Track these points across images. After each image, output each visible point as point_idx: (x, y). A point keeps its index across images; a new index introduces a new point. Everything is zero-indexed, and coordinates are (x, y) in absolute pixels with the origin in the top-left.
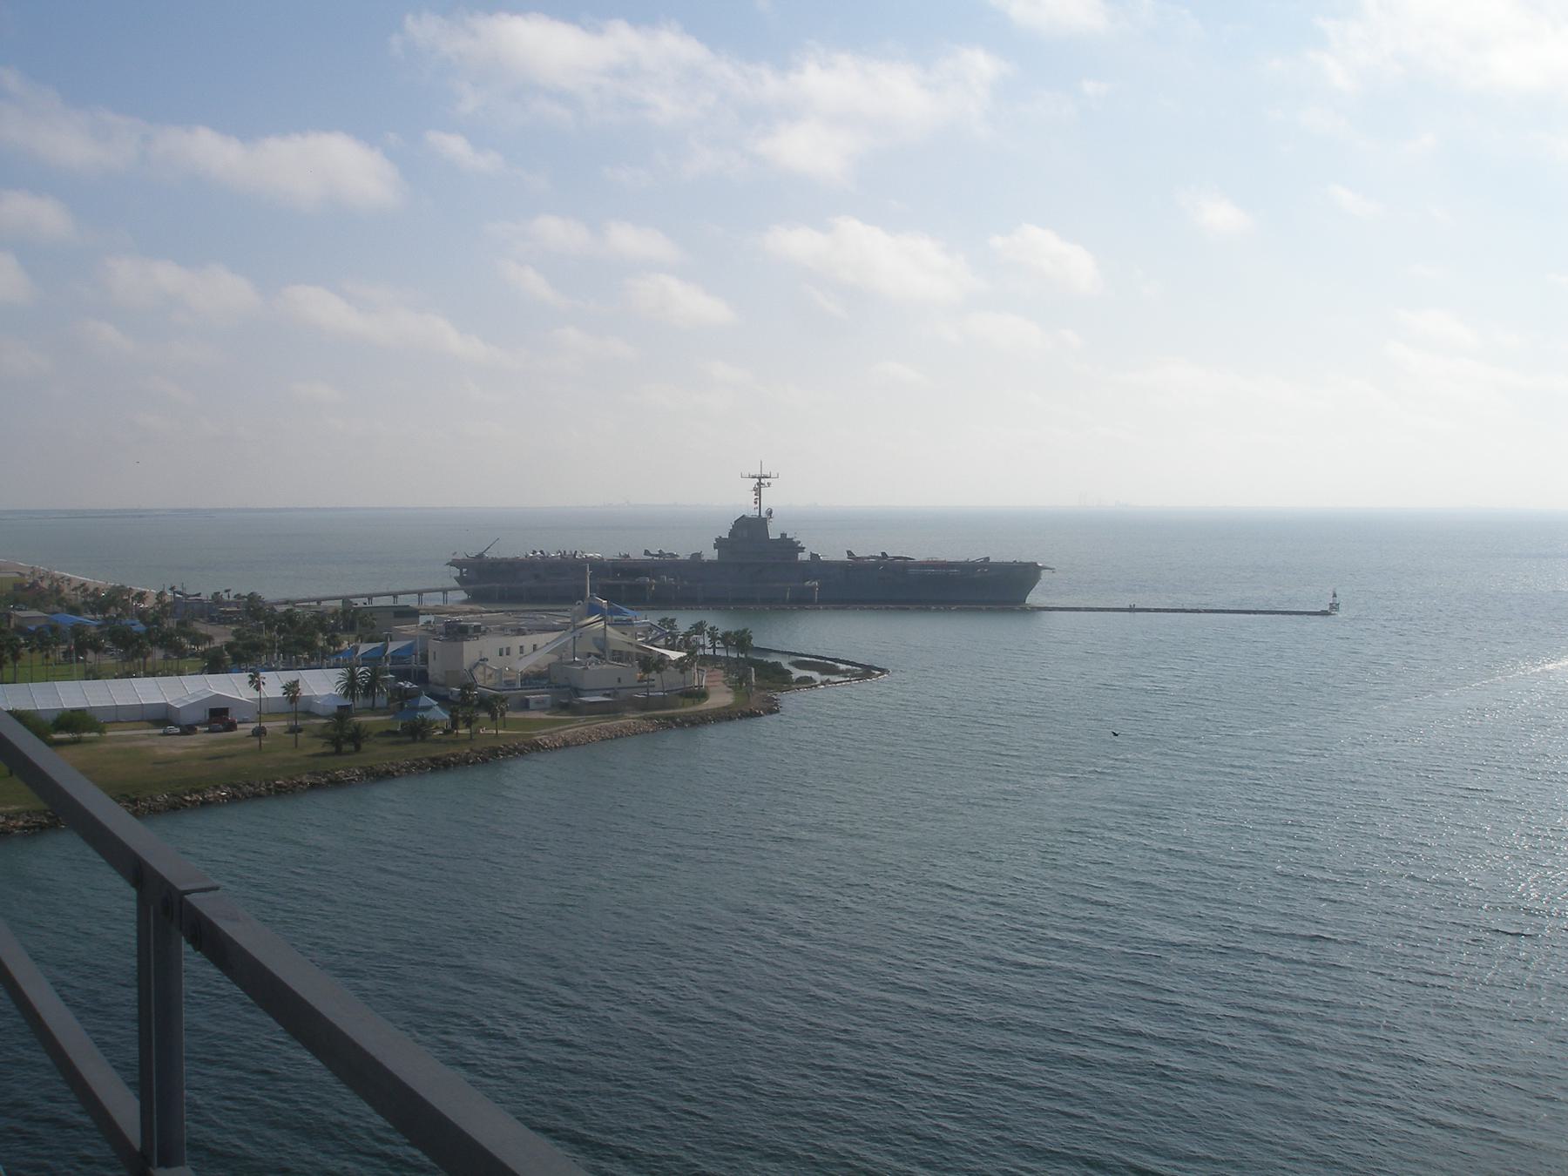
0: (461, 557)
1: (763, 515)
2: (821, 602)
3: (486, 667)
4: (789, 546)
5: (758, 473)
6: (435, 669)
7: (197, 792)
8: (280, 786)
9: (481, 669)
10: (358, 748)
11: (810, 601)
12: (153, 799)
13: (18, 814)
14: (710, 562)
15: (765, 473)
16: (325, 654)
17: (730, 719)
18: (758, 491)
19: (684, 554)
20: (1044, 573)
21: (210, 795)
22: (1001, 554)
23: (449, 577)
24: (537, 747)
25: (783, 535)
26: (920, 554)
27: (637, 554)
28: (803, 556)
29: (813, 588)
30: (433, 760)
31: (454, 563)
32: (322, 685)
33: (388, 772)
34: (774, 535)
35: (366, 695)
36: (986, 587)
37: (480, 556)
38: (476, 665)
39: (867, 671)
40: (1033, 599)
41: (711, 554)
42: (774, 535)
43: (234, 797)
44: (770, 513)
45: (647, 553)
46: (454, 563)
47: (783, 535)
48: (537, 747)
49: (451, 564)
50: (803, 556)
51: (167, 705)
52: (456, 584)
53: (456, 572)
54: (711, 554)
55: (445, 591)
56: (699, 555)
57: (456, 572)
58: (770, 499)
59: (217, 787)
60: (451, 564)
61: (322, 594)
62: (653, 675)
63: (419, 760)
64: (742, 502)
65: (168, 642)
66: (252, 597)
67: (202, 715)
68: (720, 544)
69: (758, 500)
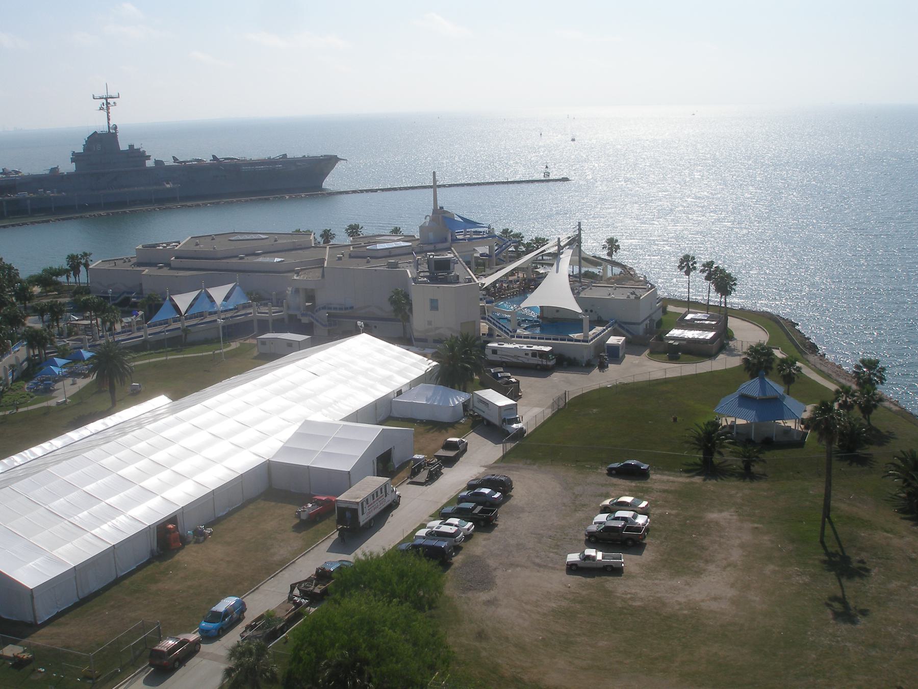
4: (136, 156)
5: (104, 95)
14: (69, 176)
22: (296, 151)
25: (131, 147)
28: (150, 163)
34: (123, 146)
36: (297, 177)
40: (330, 183)
41: (68, 167)
42: (123, 146)
47: (131, 147)
50: (150, 163)
68: (76, 158)
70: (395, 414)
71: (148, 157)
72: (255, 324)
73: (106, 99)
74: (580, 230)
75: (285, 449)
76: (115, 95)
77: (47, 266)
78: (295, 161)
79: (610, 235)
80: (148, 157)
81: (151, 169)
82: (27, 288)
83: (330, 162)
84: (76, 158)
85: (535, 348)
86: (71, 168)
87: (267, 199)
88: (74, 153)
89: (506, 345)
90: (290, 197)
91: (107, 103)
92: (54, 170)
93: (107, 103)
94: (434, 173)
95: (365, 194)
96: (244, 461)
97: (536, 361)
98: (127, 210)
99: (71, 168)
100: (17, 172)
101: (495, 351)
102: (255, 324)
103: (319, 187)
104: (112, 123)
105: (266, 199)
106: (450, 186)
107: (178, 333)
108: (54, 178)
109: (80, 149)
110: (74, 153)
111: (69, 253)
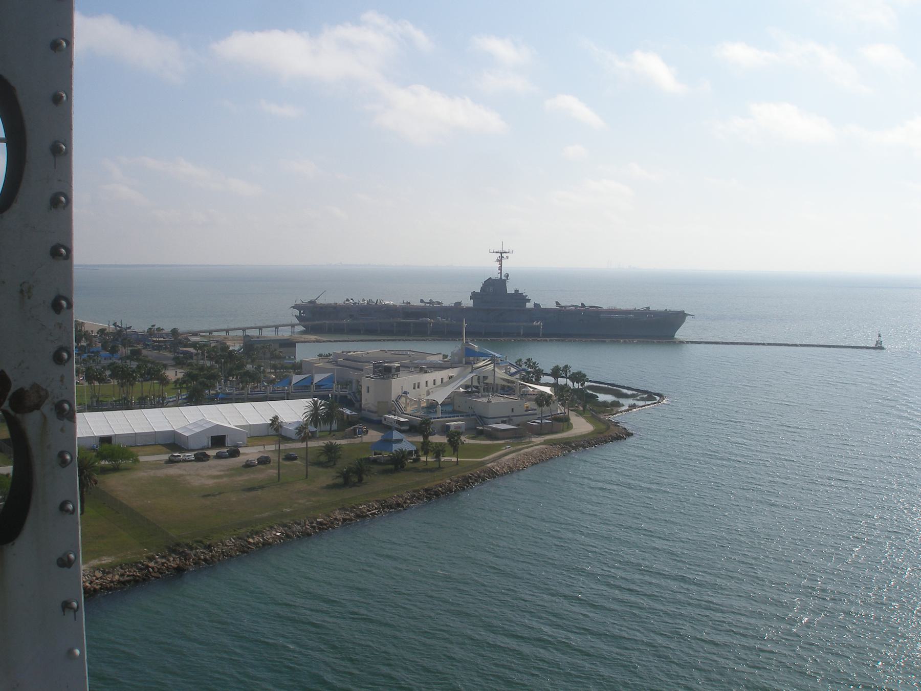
0: (299, 302)
1: (503, 278)
2: (544, 335)
3: (407, 398)
4: (520, 298)
5: (500, 250)
6: (368, 400)
7: (257, 533)
8: (321, 523)
9: (403, 400)
10: (360, 480)
11: (537, 335)
12: (224, 544)
13: (113, 567)
14: (468, 309)
16: (253, 377)
17: (606, 442)
18: (500, 261)
19: (448, 302)
20: (688, 317)
21: (268, 536)
22: (658, 305)
23: (291, 316)
24: (493, 474)
25: (517, 291)
27: (416, 302)
28: (529, 305)
29: (538, 327)
30: (426, 490)
32: (293, 412)
33: (398, 505)
34: (510, 290)
35: (325, 422)
36: (654, 327)
37: (311, 302)
38: (400, 397)
39: (651, 396)
40: (680, 335)
41: (468, 303)
42: (510, 290)
43: (288, 536)
45: (422, 301)
47: (517, 291)
48: (493, 474)
50: (529, 305)
51: (174, 433)
52: (297, 322)
53: (297, 312)
54: (468, 303)
55: (293, 326)
56: (460, 303)
59: (272, 527)
61: (212, 328)
62: (545, 408)
63: (417, 491)
64: (488, 267)
66: (174, 332)
67: (207, 442)
68: (474, 296)
69: (500, 269)
71: (529, 301)
78: (657, 313)
80: (529, 301)
81: (530, 310)
82: (159, 371)
84: (474, 296)
86: (469, 303)
87: (604, 342)
91: (501, 256)
93: (501, 256)
95: (761, 346)
96: (168, 428)
99: (469, 303)
100: (439, 303)
108: (457, 310)
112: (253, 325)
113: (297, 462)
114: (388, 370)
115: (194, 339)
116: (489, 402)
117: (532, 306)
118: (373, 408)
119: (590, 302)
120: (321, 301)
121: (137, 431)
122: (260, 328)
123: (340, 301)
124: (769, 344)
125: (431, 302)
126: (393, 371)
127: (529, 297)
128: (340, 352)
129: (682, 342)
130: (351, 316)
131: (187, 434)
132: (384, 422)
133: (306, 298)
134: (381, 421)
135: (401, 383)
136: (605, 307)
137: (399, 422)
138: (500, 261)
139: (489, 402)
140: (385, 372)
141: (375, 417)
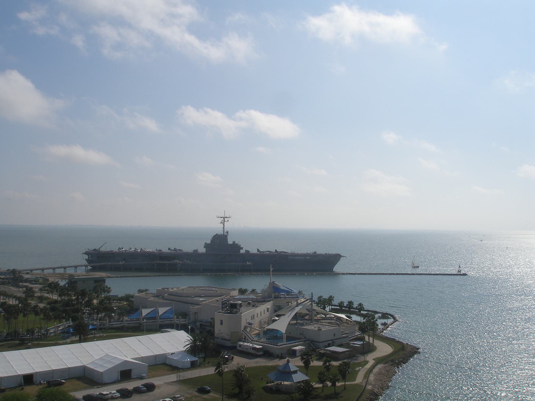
0: (87, 250)
1: (225, 234)
4: (236, 247)
15: (226, 216)
18: (223, 223)
22: (321, 251)
23: (82, 260)
25: (234, 242)
26: (150, 248)
27: (165, 250)
28: (242, 251)
31: (86, 253)
34: (230, 242)
36: (321, 264)
38: (245, 328)
40: (337, 268)
41: (202, 250)
42: (230, 242)
44: (228, 232)
45: (169, 249)
46: (86, 253)
47: (234, 242)
49: (85, 253)
50: (242, 251)
51: (84, 369)
53: (86, 257)
54: (202, 250)
55: (86, 266)
57: (86, 257)
58: (228, 226)
60: (85, 253)
64: (216, 227)
65: (54, 312)
66: (14, 269)
67: (116, 376)
68: (206, 246)
70: (167, 363)
71: (242, 248)
72: (175, 325)
73: (224, 218)
74: (312, 296)
75: (93, 363)
76: (228, 216)
77: (128, 293)
79: (360, 302)
80: (242, 248)
81: (242, 254)
83: (337, 257)
84: (206, 246)
85: (255, 346)
88: (206, 244)
89: (246, 344)
90: (308, 274)
91: (224, 219)
92: (196, 251)
93: (224, 219)
94: (418, 267)
97: (253, 352)
98: (221, 274)
100: (180, 250)
101: (240, 346)
102: (175, 325)
103: (331, 270)
104: (225, 231)
105: (294, 274)
106: (369, 274)
107: (137, 325)
108: (195, 254)
109: (209, 242)
110: (206, 244)
111: (139, 289)
112: (60, 266)
113: (212, 394)
114: (234, 306)
115: (26, 276)
116: (320, 330)
117: (244, 252)
118: (227, 337)
119: (281, 248)
120: (103, 249)
121: (54, 368)
122: (65, 268)
123: (116, 250)
124: (397, 274)
125: (175, 250)
126: (238, 307)
127: (242, 246)
128: (160, 288)
129: (339, 274)
130: (124, 259)
131: (101, 370)
132: (238, 348)
133: (92, 247)
134: (236, 347)
135: (246, 314)
136: (289, 252)
137: (254, 349)
138: (223, 223)
139: (320, 330)
140: (232, 308)
141: (228, 344)
